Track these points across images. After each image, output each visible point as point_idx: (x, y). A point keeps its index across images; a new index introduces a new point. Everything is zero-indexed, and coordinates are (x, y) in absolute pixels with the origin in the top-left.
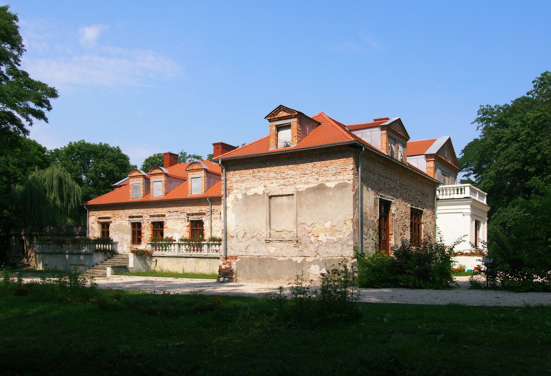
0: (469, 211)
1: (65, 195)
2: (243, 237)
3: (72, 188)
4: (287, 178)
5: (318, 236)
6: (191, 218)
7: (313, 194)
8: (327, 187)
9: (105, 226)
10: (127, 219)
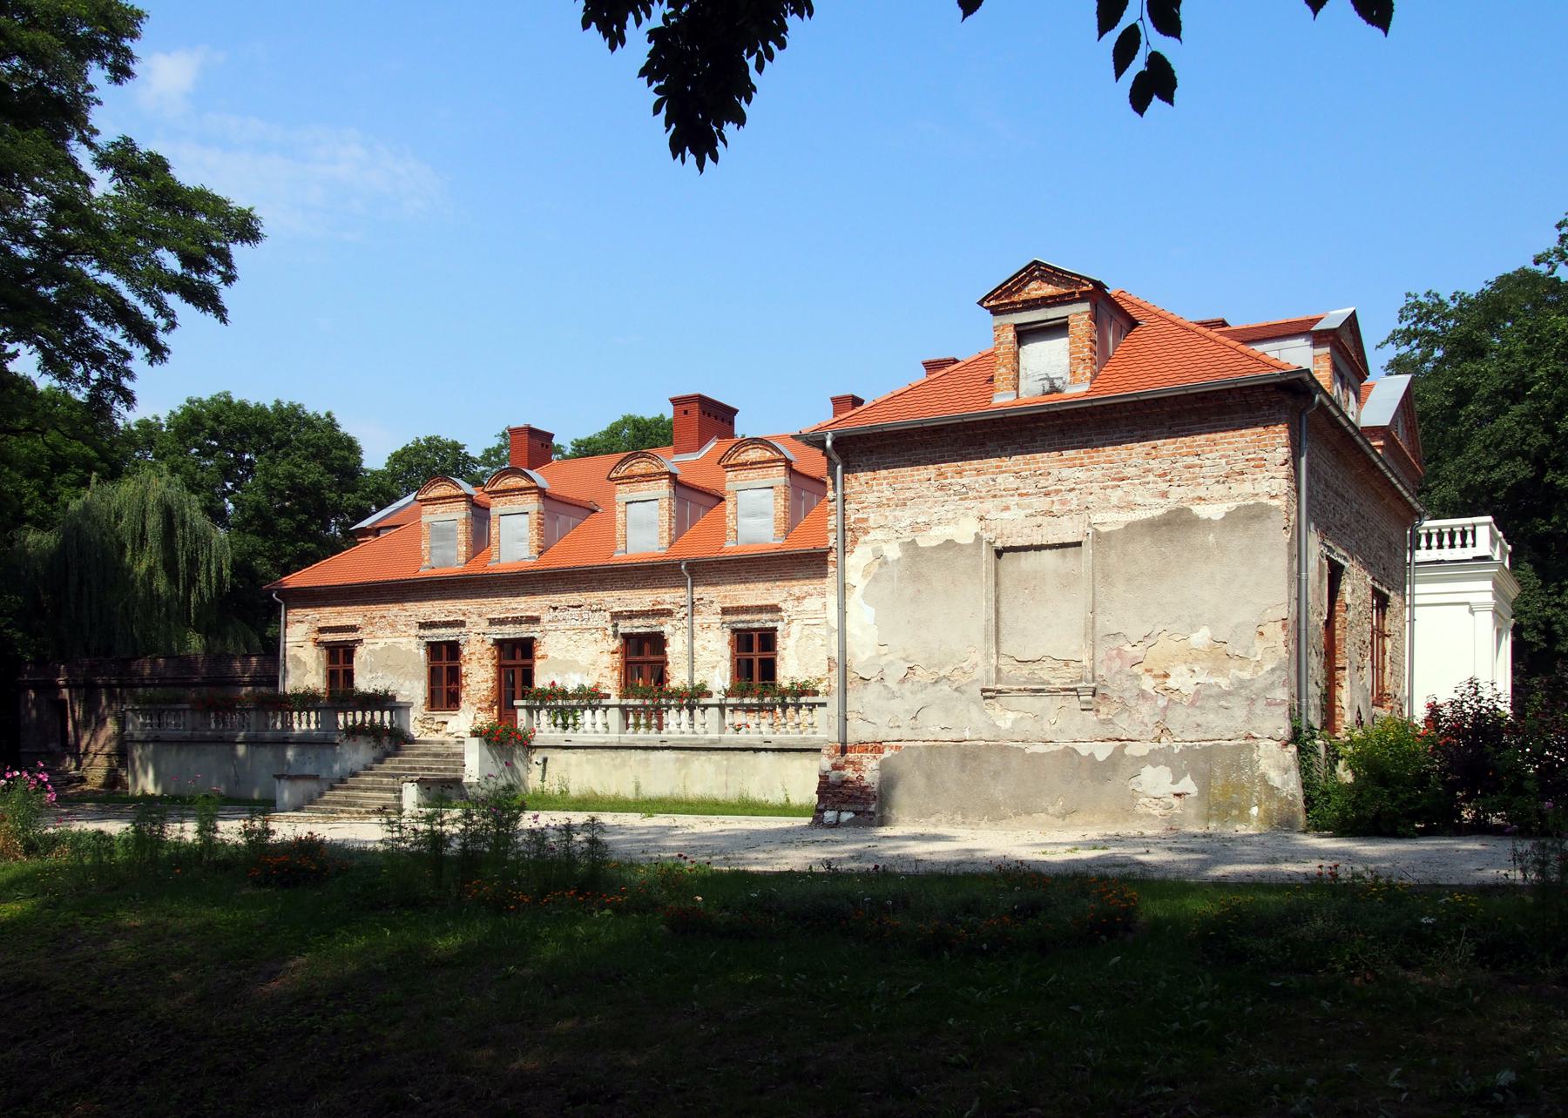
0: (1488, 598)
1: (182, 559)
2: (904, 680)
3: (202, 539)
4: (1058, 492)
5: (1166, 676)
6: (625, 627)
7: (1148, 540)
8: (1197, 519)
9: (340, 656)
10: (414, 632)
